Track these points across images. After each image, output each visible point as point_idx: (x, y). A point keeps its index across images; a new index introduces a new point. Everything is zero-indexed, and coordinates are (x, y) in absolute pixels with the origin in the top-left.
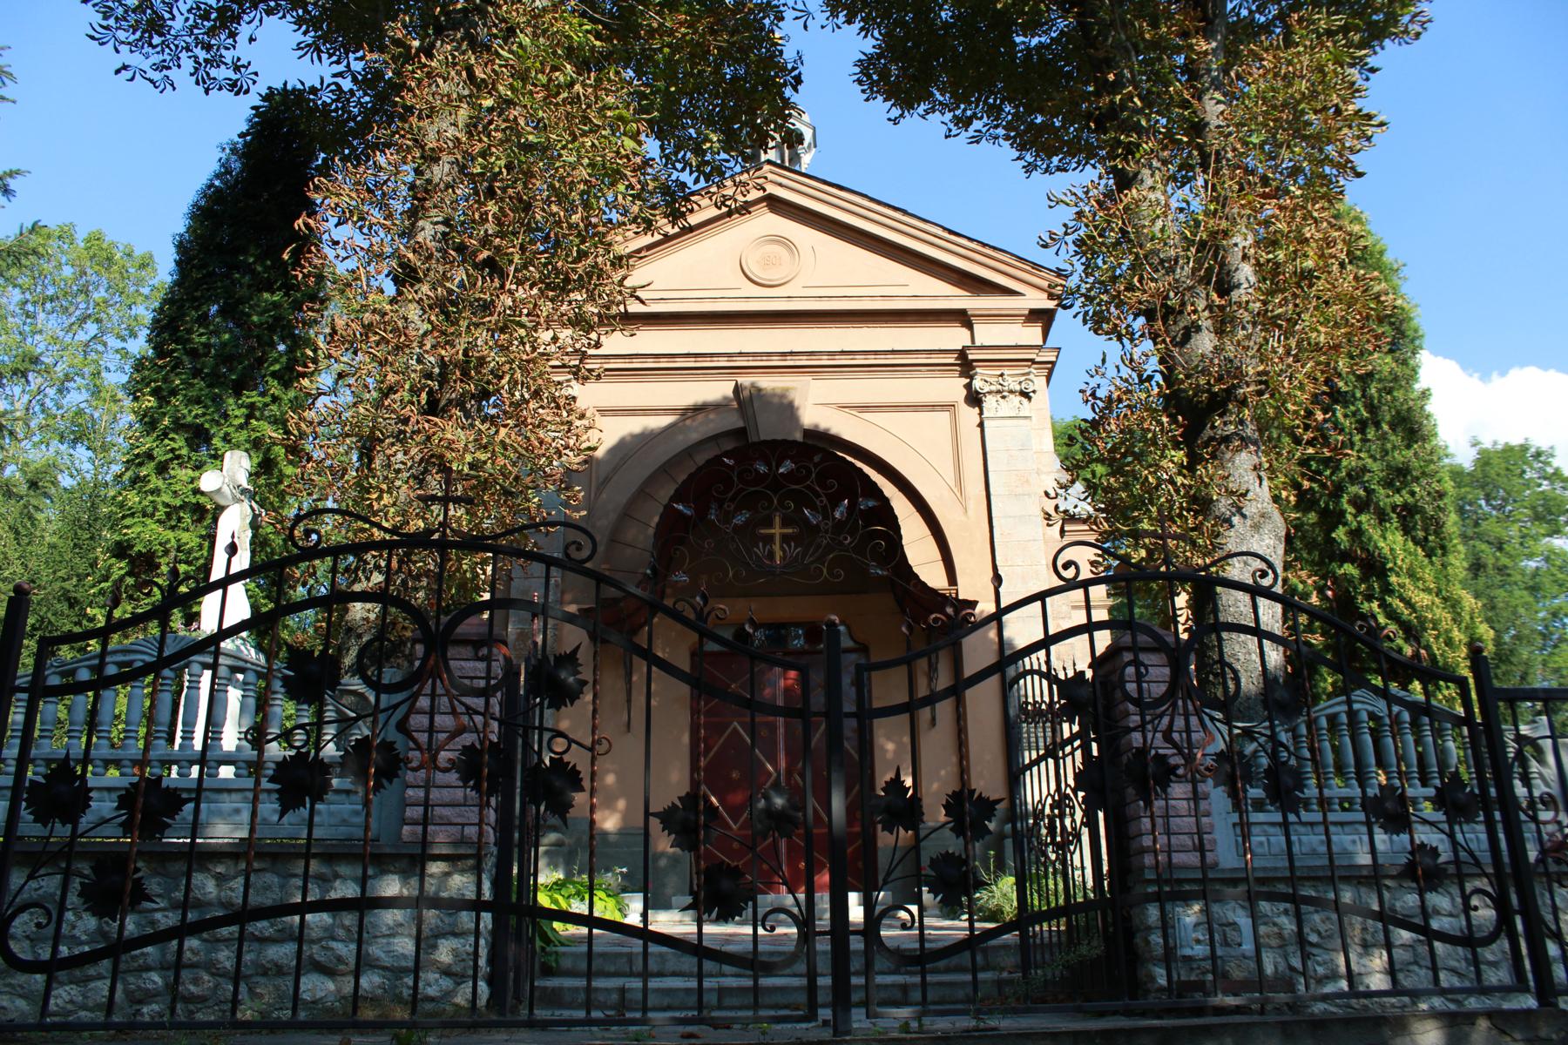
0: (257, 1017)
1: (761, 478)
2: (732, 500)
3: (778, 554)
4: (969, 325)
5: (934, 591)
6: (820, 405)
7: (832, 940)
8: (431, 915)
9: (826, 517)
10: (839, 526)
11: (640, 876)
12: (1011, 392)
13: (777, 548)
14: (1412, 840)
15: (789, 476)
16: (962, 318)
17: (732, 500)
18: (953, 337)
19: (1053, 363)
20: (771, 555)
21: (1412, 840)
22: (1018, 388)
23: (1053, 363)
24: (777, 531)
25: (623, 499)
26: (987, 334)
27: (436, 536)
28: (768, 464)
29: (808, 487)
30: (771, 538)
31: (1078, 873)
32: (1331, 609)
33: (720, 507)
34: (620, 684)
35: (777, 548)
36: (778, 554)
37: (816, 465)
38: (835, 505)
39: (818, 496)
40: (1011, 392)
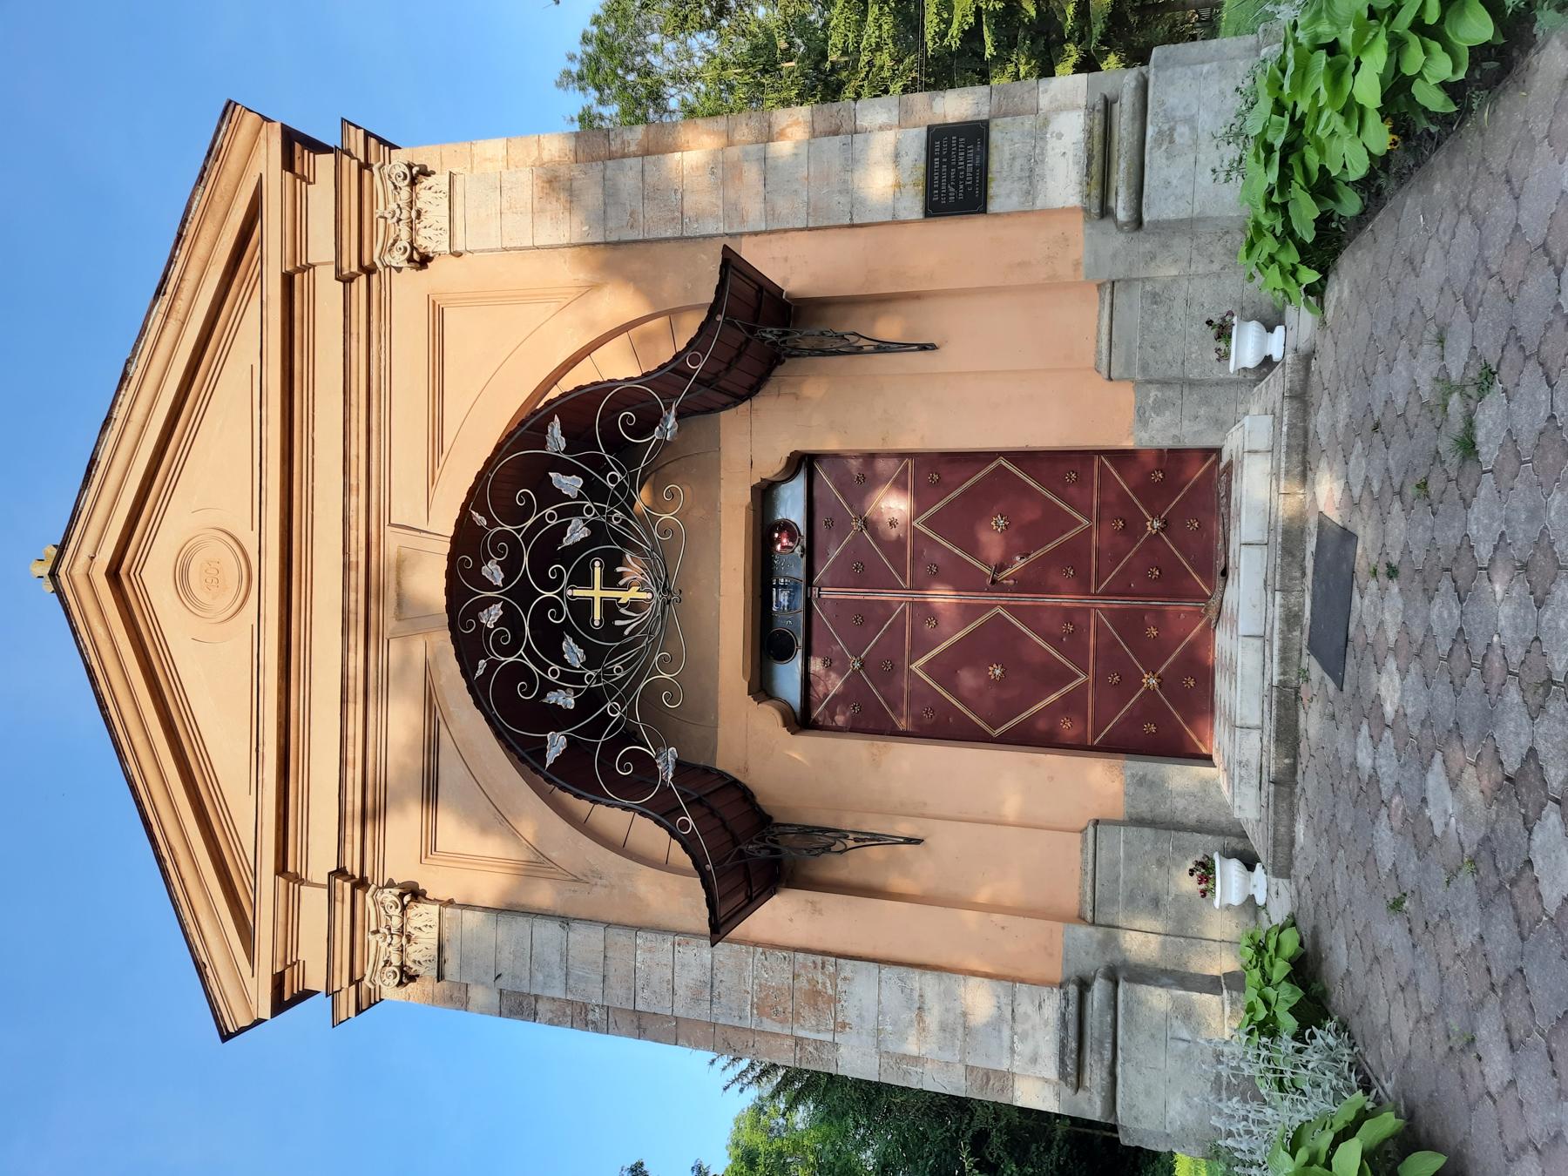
2: (544, 668)
5: (421, 144)
6: (425, 513)
8: (1154, 393)
9: (576, 511)
10: (593, 489)
12: (411, 204)
15: (510, 568)
17: (544, 668)
18: (327, 291)
19: (367, 135)
20: (634, 606)
22: (405, 193)
23: (367, 135)
24: (597, 593)
26: (320, 248)
28: (491, 601)
29: (527, 539)
30: (610, 607)
33: (555, 687)
34: (876, 852)
35: (625, 597)
37: (492, 523)
38: (559, 496)
39: (541, 523)
40: (411, 204)
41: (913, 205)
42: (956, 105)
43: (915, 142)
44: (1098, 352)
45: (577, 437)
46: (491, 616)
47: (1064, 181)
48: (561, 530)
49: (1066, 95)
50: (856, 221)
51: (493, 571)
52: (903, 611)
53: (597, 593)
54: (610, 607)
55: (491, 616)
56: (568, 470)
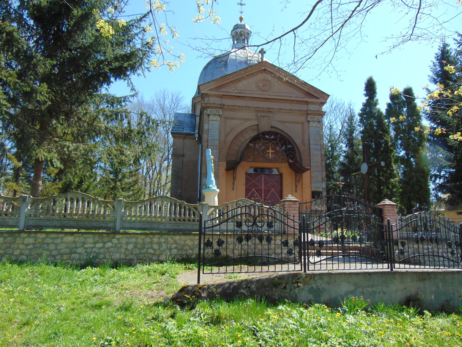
0: (155, 236)
1: (267, 139)
3: (271, 156)
4: (307, 104)
7: (257, 265)
9: (280, 149)
11: (136, 236)
13: (270, 155)
14: (262, 58)
16: (307, 103)
18: (304, 107)
20: (269, 156)
21: (262, 58)
24: (270, 151)
25: (232, 138)
27: (34, 95)
28: (269, 136)
30: (269, 153)
31: (385, 236)
32: (448, 182)
35: (270, 155)
36: (271, 156)
41: (314, 189)
42: (324, 194)
43: (320, 190)
44: (141, 234)
45: (289, 149)
46: (267, 137)
47: (314, 208)
48: (278, 147)
49: (324, 208)
50: (279, 39)
51: (273, 137)
52: (259, 187)
53: (270, 151)
54: (269, 153)
55: (267, 137)
56: (286, 148)
